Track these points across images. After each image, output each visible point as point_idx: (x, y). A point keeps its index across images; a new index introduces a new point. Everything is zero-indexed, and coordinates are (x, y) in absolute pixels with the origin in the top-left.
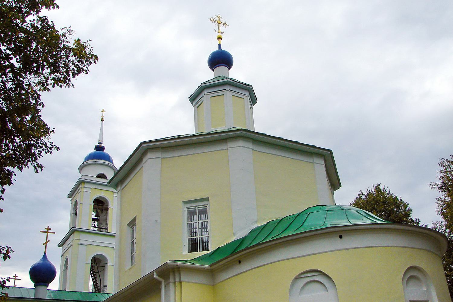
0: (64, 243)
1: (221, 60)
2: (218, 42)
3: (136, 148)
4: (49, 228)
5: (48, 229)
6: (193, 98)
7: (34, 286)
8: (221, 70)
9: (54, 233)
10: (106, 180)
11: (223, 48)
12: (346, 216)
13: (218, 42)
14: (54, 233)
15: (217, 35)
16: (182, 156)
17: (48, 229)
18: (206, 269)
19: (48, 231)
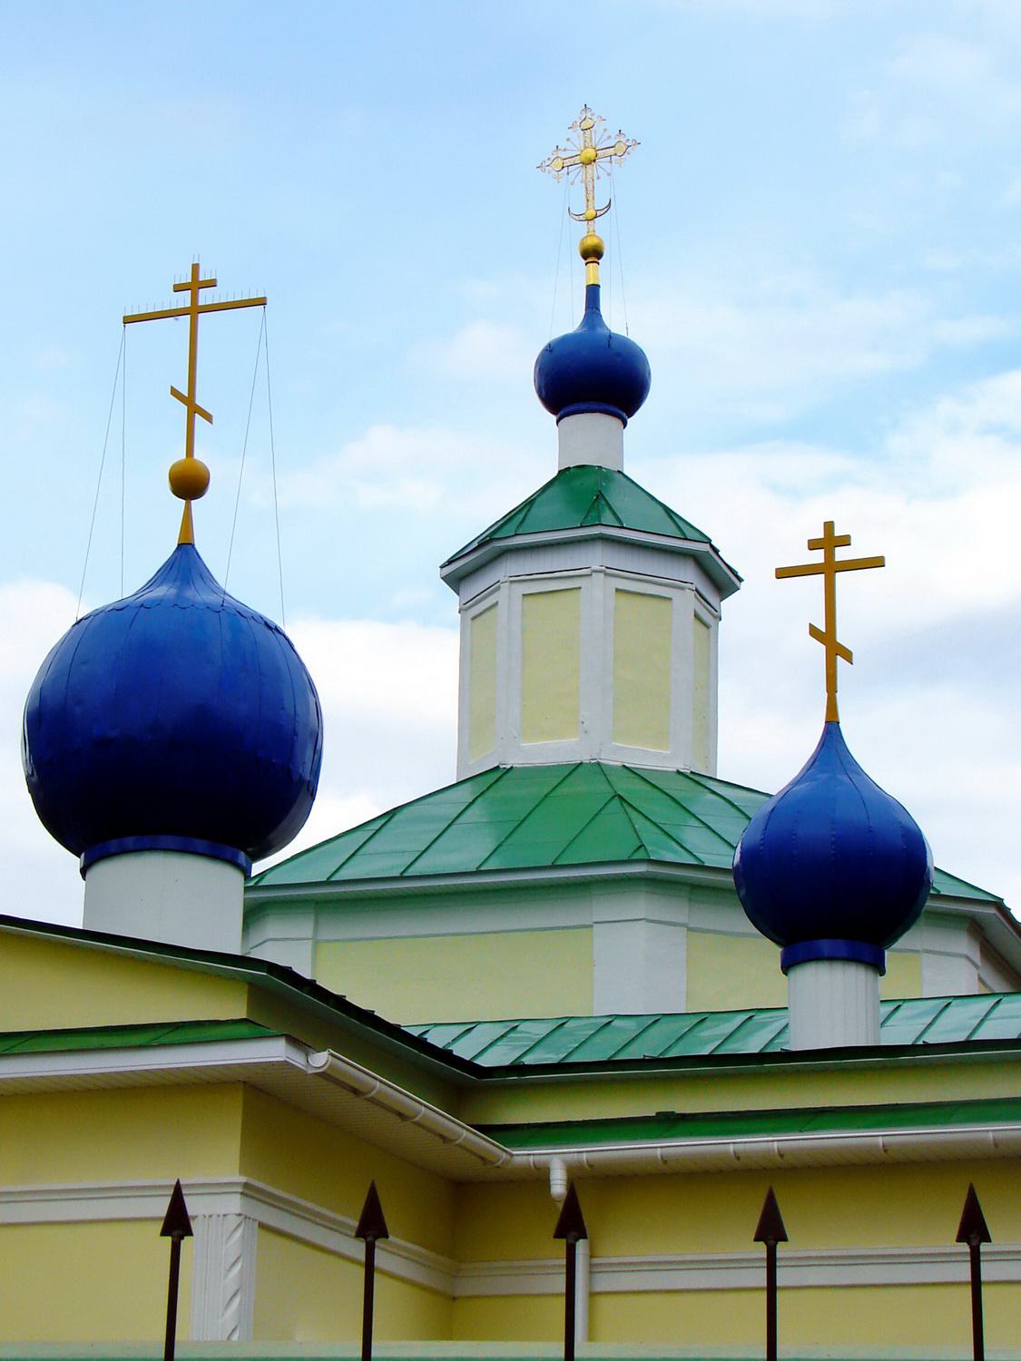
0: (365, 823)
1: (592, 378)
2: (583, 275)
3: (29, 795)
4: (838, 533)
5: (830, 540)
6: (468, 569)
7: (959, 1239)
8: (590, 435)
9: (877, 562)
10: (177, 388)
11: (615, 320)
12: (603, 777)
13: (583, 275)
14: (877, 562)
15: (579, 234)
16: (400, 937)
17: (830, 540)
18: (460, 1146)
19: (829, 555)
